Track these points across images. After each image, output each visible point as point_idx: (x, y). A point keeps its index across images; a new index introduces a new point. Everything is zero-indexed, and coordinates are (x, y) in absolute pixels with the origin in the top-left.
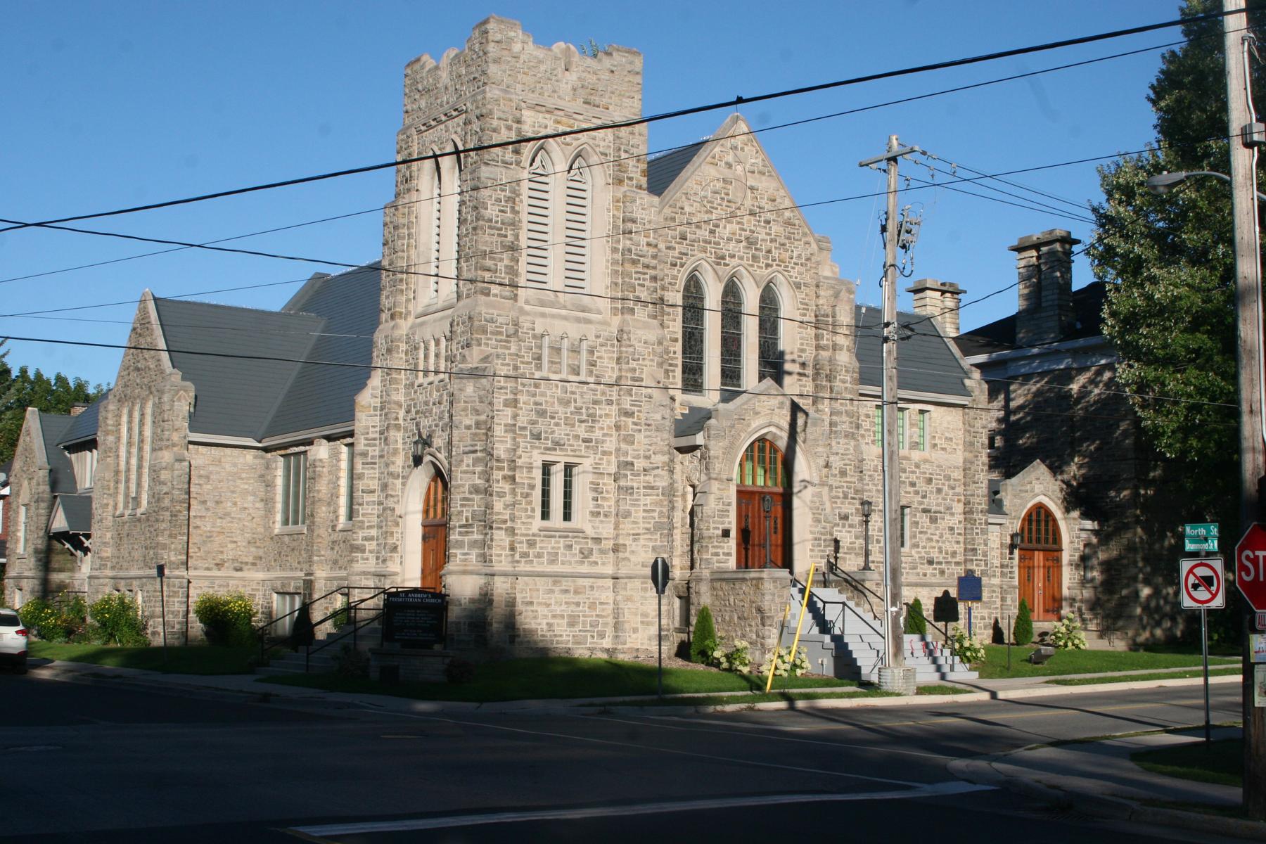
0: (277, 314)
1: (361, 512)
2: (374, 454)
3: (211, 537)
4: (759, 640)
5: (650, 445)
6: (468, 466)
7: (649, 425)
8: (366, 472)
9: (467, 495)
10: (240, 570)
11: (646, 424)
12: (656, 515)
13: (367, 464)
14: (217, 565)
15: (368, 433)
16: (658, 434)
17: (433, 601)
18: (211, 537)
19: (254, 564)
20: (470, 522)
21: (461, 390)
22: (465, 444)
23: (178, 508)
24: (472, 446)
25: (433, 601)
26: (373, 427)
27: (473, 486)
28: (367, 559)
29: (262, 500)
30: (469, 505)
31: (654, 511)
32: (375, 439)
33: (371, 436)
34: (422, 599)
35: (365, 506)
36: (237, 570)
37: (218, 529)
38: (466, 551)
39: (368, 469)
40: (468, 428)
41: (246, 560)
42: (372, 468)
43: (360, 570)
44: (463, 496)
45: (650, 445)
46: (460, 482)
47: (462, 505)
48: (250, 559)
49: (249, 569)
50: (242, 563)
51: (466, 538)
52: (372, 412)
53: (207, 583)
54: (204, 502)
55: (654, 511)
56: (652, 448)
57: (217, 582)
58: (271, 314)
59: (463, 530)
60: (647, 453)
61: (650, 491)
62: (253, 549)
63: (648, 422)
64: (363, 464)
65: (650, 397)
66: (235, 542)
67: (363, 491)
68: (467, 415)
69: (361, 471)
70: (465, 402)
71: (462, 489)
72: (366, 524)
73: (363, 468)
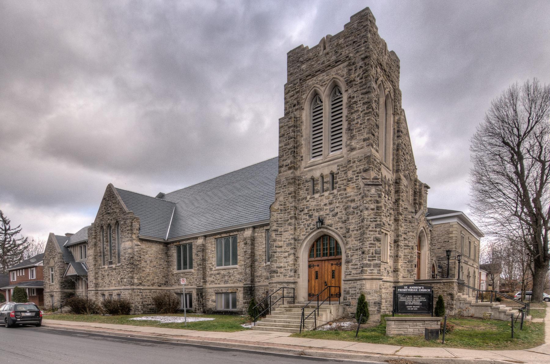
0: (154, 198)
1: (275, 256)
2: (281, 230)
3: (149, 274)
4: (448, 306)
5: (407, 228)
6: (373, 228)
7: (406, 220)
8: (278, 238)
9: (372, 242)
10: (160, 286)
11: (405, 220)
12: (409, 257)
13: (278, 235)
14: (152, 284)
15: (278, 221)
16: (410, 224)
17: (425, 290)
18: (149, 274)
19: (165, 284)
20: (374, 255)
21: (368, 190)
22: (371, 217)
23: (137, 263)
24: (375, 218)
25: (425, 290)
26: (280, 218)
27: (376, 238)
28: (279, 276)
29: (167, 262)
30: (373, 247)
31: (408, 255)
32: (281, 224)
33: (279, 222)
34: (418, 289)
35: (277, 253)
36: (159, 286)
37: (152, 272)
38: (372, 268)
39: (278, 237)
40: (373, 209)
41: (162, 282)
42: (280, 237)
43: (275, 281)
44: (370, 242)
45: (407, 228)
46: (368, 236)
47: (370, 247)
48: (164, 282)
49: (163, 286)
50: (161, 284)
51: (372, 263)
52: (279, 212)
53: (148, 291)
54: (146, 262)
55: (408, 255)
56: (408, 230)
57: (152, 291)
58: (152, 198)
59: (371, 258)
60: (405, 232)
61: (406, 248)
62: (164, 279)
63: (406, 219)
64: (276, 235)
65: (407, 209)
66: (158, 276)
67: (276, 247)
68: (372, 203)
69: (274, 238)
70: (371, 197)
71: (370, 239)
72: (278, 261)
73: (276, 237)
